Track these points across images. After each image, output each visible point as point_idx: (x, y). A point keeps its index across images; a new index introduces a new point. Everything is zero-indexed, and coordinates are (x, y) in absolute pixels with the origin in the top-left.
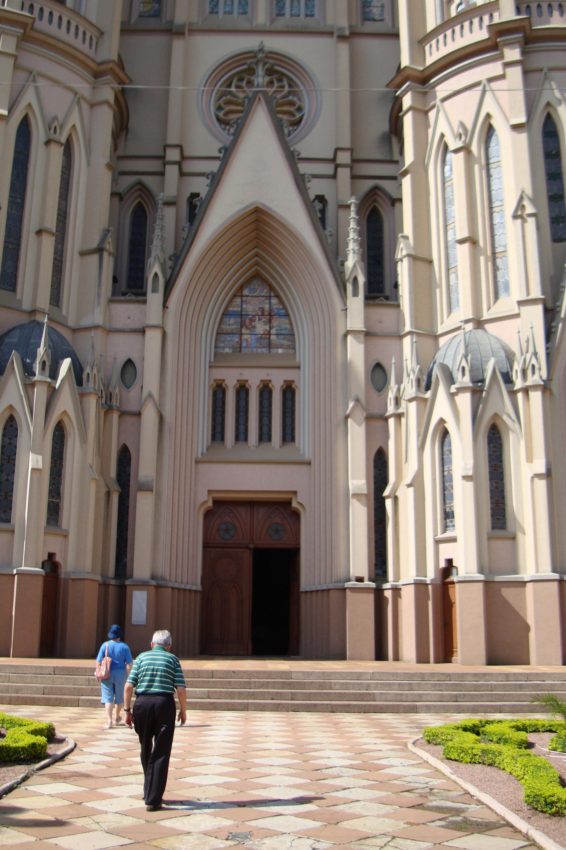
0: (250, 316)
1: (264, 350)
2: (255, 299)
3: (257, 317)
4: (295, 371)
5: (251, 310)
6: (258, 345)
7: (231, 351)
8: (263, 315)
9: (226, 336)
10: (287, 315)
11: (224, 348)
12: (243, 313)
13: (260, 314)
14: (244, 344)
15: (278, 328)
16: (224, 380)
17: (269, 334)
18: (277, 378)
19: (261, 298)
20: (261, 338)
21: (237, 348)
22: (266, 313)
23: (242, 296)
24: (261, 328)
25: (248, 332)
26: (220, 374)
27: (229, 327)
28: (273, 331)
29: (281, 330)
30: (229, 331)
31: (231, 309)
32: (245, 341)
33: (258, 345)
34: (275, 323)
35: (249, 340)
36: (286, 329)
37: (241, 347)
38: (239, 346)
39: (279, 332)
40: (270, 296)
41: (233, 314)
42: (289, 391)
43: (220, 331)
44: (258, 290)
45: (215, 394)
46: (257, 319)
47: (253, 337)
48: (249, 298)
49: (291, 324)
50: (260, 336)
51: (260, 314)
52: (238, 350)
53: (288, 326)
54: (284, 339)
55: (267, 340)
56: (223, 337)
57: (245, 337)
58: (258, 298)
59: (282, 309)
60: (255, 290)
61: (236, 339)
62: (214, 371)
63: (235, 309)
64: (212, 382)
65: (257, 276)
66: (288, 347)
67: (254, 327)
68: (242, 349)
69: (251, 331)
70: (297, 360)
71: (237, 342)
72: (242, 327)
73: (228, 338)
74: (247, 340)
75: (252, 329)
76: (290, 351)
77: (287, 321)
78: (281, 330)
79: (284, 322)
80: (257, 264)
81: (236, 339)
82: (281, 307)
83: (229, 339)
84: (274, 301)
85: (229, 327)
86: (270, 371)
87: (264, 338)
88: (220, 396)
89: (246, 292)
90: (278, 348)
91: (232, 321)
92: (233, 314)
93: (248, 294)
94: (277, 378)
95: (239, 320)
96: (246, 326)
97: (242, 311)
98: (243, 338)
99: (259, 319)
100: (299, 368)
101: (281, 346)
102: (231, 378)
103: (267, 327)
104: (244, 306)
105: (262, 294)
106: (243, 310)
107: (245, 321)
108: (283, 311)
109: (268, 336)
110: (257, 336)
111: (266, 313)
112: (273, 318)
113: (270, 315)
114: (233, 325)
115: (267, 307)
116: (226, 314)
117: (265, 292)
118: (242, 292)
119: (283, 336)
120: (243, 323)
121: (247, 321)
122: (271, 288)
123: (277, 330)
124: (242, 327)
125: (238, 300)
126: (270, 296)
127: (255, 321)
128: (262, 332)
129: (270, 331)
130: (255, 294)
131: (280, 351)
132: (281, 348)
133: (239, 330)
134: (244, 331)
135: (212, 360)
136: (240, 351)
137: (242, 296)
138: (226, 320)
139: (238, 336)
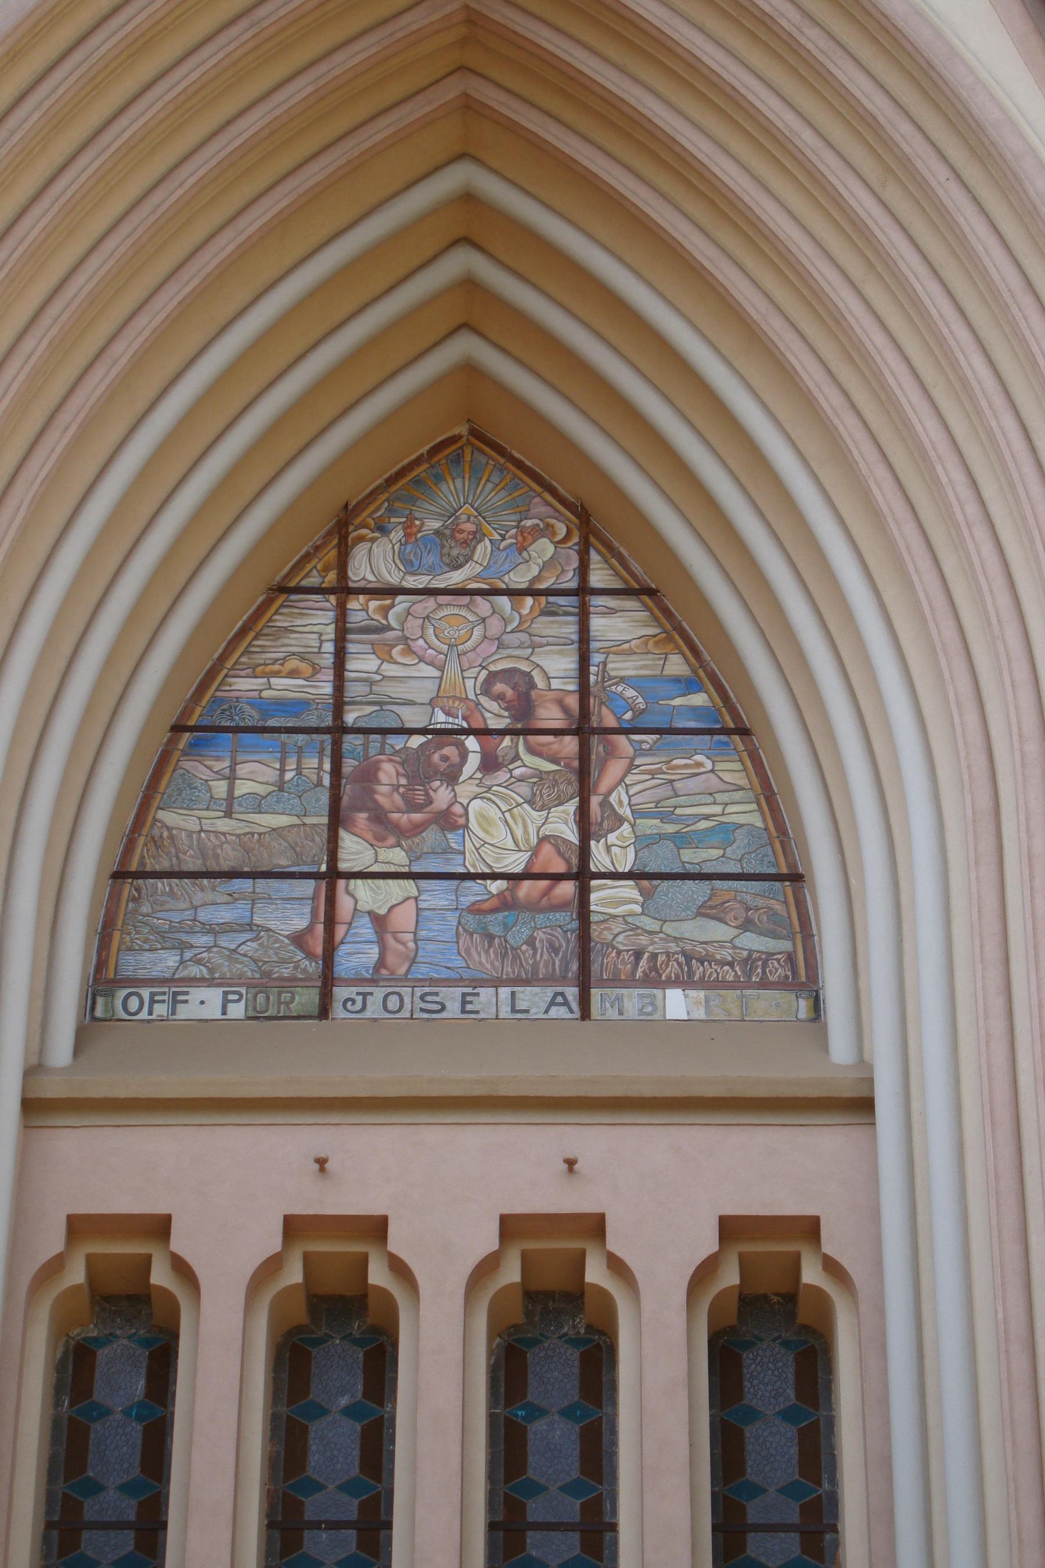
0: (416, 741)
1: (534, 999)
2: (450, 609)
3: (472, 743)
4: (828, 1141)
5: (424, 692)
6: (485, 962)
7: (237, 1010)
8: (524, 728)
9: (202, 892)
10: (735, 726)
11: (175, 986)
12: (350, 718)
13: (496, 717)
14: (357, 955)
15: (650, 826)
16: (159, 1227)
17: (583, 875)
18: (662, 1210)
19: (504, 601)
20: (505, 904)
21: (289, 983)
22: (550, 716)
23: (344, 590)
24: (504, 824)
25: (396, 858)
26: (116, 1169)
27: (224, 825)
28: (611, 852)
29: (681, 840)
30: (229, 858)
31: (244, 685)
32: (365, 929)
33: (485, 962)
34: (629, 783)
35: (404, 919)
36: (726, 832)
37: (328, 981)
38: (313, 968)
39: (659, 860)
40: (583, 591)
41: (265, 727)
42: (772, 1328)
43: (143, 857)
44: (483, 550)
45: (76, 1369)
46: (474, 761)
47: (437, 896)
48: (402, 603)
49: (770, 793)
50: (496, 886)
51: (496, 717)
52: (307, 998)
53: (746, 814)
54: (708, 911)
55: (568, 919)
56: (170, 904)
57: (364, 896)
58: (483, 605)
59: (690, 685)
60: (455, 545)
61: (289, 912)
62: (71, 1144)
63: (283, 687)
64: (52, 1240)
65: (470, 438)
66: (751, 973)
67: (449, 821)
68: (341, 993)
69: (414, 856)
70: (841, 1049)
71: (299, 939)
72: (336, 820)
73: (218, 905)
74: (379, 922)
75: (431, 836)
76: (768, 1004)
77: (732, 771)
78: (681, 840)
79: (710, 788)
80: (473, 308)
81: (289, 912)
82: (677, 665)
83: (225, 915)
84: (617, 625)
85: (224, 825)
86: (593, 1140)
87: (533, 907)
88: (122, 1383)
89: (373, 561)
90: (654, 980)
91: (256, 774)
92: (265, 727)
93: (393, 577)
94: (662, 1210)
95: (316, 765)
96: (379, 817)
97: (339, 703)
98: (345, 904)
99: (490, 764)
100: (863, 1106)
101: (689, 970)
102: (227, 1204)
103: (563, 824)
104: (362, 663)
105: (519, 579)
106: (353, 690)
107: (369, 775)
108: (699, 699)
109: (567, 889)
110: (473, 892)
111: (550, 716)
112: (611, 752)
113: (582, 728)
114: (259, 804)
115: (557, 667)
116: (195, 724)
117: (544, 559)
118: (342, 565)
119: (699, 890)
120: (348, 791)
121: (388, 773)
122: (592, 521)
123: (644, 843)
124: (336, 820)
125: (313, 624)
126: (583, 591)
127: (452, 777)
128: (515, 863)
129: (584, 852)
130: (455, 578)
131: (677, 1004)
132: (685, 982)
133: (321, 838)
134: (355, 852)
135: (61, 1049)
136: (324, 1012)
137: (344, 590)
138: (206, 771)
139: (308, 887)
